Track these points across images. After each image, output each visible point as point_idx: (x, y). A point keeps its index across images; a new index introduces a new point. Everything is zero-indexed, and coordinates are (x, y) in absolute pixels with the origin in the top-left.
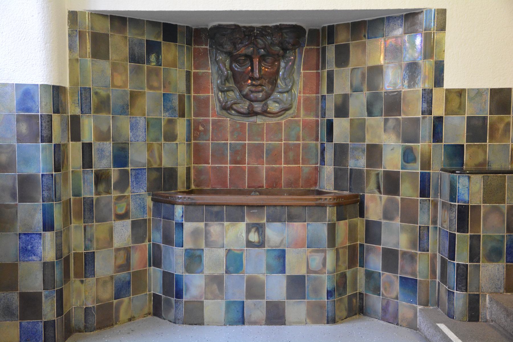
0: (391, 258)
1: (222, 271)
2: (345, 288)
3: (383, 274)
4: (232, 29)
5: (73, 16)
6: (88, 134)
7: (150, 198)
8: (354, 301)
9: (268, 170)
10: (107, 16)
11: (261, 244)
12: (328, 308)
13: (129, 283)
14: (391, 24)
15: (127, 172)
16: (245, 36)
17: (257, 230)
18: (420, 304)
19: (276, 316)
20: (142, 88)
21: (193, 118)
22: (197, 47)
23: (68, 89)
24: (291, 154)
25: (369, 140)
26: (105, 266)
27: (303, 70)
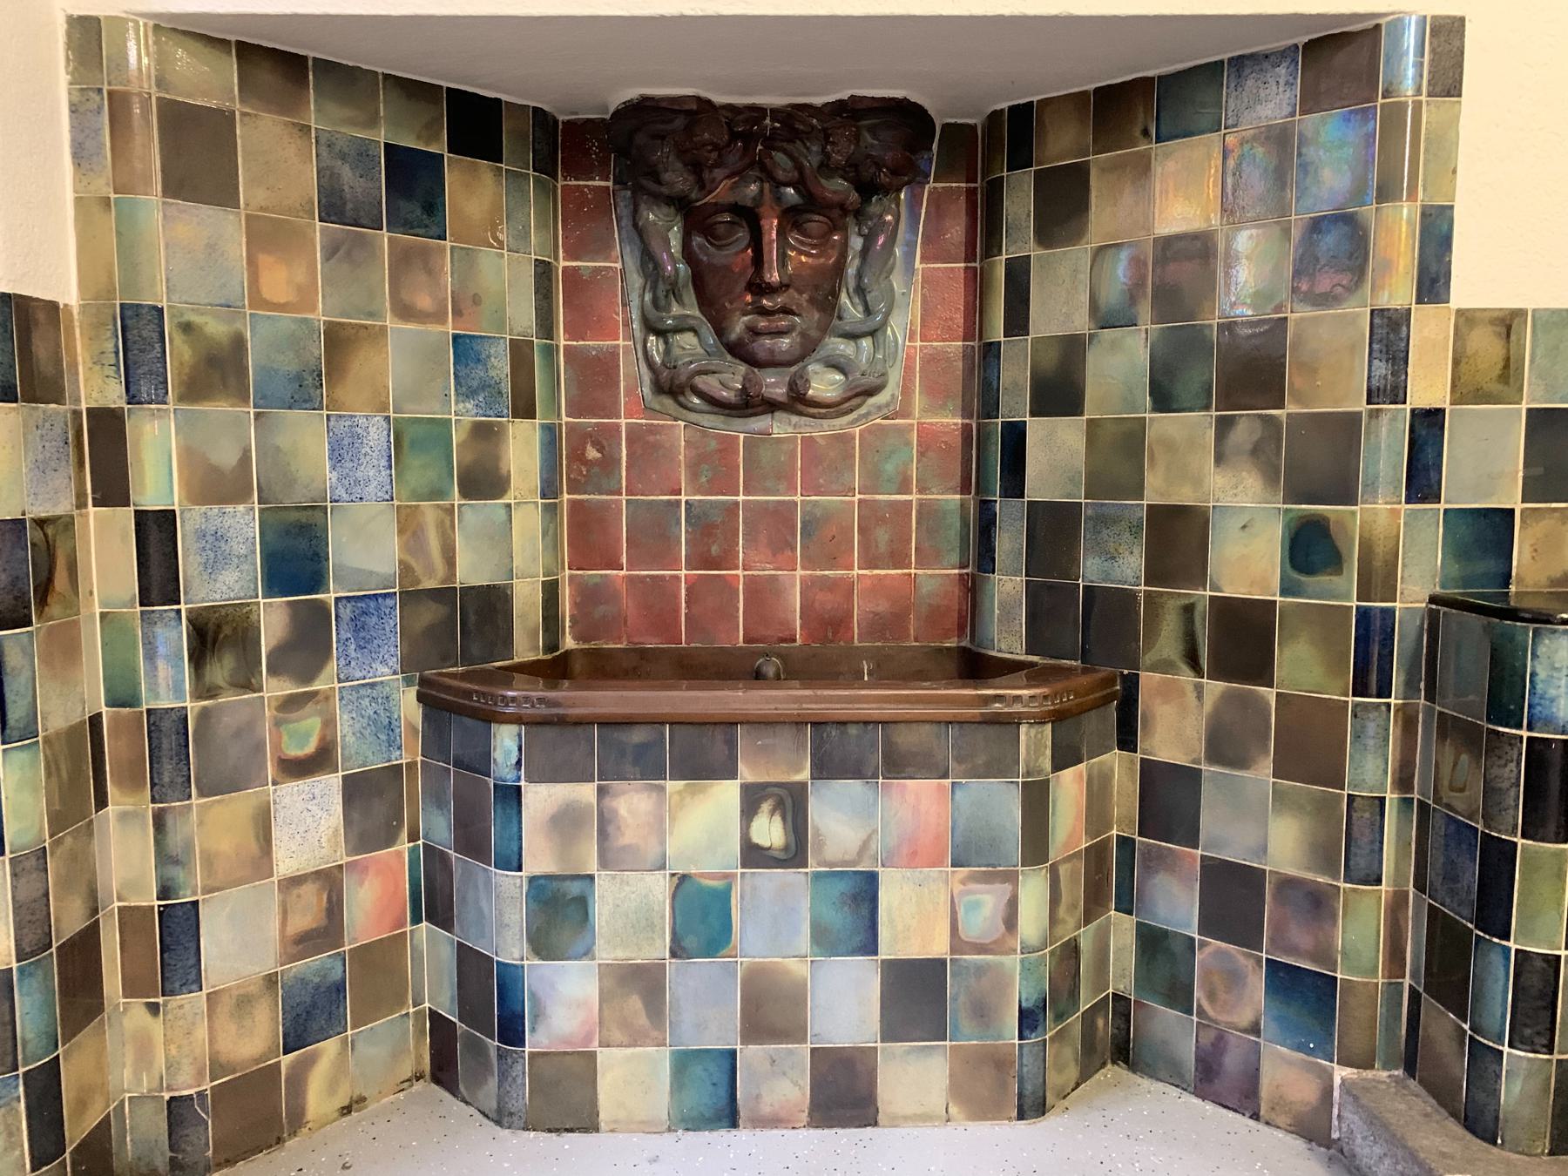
0: (1233, 896)
1: (658, 949)
2: (1074, 994)
3: (1203, 944)
4: (688, 113)
5: (87, 36)
6: (157, 478)
7: (412, 693)
8: (1100, 1023)
9: (808, 586)
10: (223, 43)
11: (795, 854)
12: (1021, 1065)
13: (339, 988)
14: (1250, 83)
15: (322, 608)
16: (734, 136)
17: (779, 807)
18: (1345, 1062)
19: (844, 1095)
20: (371, 315)
21: (565, 419)
22: (574, 183)
23: (75, 312)
24: (882, 536)
25: (1158, 489)
26: (240, 942)
27: (924, 259)
